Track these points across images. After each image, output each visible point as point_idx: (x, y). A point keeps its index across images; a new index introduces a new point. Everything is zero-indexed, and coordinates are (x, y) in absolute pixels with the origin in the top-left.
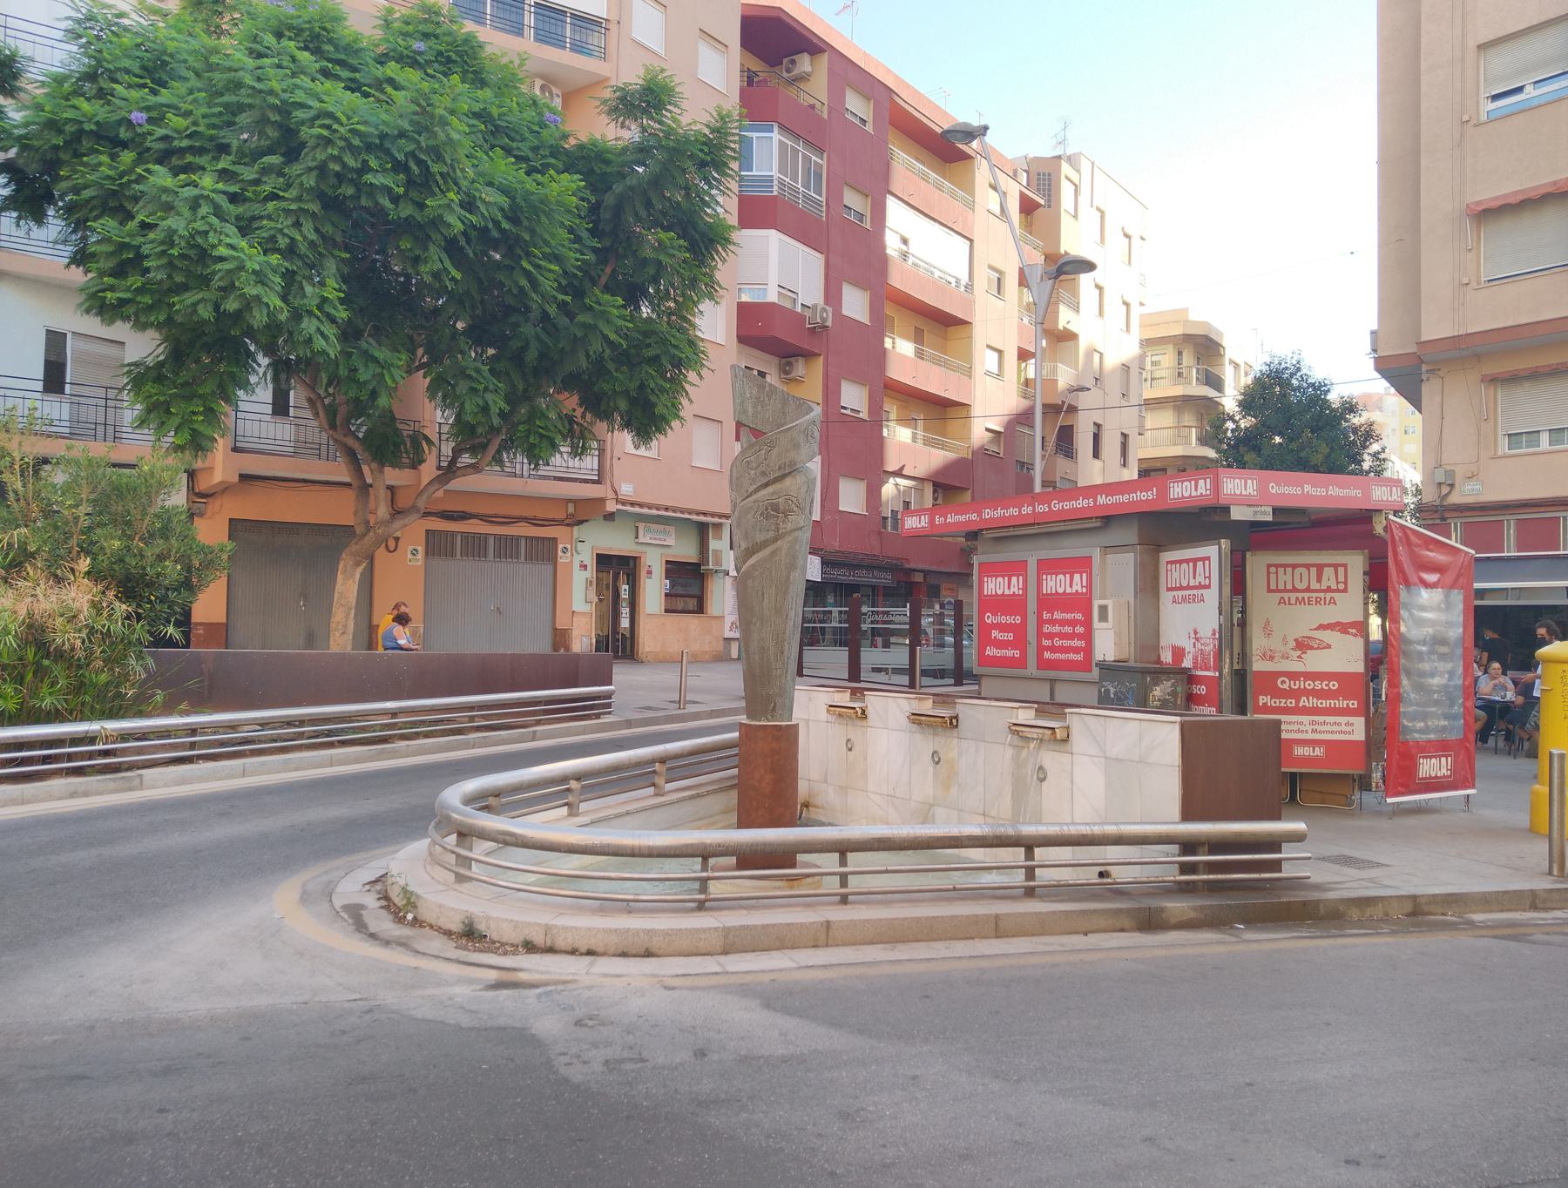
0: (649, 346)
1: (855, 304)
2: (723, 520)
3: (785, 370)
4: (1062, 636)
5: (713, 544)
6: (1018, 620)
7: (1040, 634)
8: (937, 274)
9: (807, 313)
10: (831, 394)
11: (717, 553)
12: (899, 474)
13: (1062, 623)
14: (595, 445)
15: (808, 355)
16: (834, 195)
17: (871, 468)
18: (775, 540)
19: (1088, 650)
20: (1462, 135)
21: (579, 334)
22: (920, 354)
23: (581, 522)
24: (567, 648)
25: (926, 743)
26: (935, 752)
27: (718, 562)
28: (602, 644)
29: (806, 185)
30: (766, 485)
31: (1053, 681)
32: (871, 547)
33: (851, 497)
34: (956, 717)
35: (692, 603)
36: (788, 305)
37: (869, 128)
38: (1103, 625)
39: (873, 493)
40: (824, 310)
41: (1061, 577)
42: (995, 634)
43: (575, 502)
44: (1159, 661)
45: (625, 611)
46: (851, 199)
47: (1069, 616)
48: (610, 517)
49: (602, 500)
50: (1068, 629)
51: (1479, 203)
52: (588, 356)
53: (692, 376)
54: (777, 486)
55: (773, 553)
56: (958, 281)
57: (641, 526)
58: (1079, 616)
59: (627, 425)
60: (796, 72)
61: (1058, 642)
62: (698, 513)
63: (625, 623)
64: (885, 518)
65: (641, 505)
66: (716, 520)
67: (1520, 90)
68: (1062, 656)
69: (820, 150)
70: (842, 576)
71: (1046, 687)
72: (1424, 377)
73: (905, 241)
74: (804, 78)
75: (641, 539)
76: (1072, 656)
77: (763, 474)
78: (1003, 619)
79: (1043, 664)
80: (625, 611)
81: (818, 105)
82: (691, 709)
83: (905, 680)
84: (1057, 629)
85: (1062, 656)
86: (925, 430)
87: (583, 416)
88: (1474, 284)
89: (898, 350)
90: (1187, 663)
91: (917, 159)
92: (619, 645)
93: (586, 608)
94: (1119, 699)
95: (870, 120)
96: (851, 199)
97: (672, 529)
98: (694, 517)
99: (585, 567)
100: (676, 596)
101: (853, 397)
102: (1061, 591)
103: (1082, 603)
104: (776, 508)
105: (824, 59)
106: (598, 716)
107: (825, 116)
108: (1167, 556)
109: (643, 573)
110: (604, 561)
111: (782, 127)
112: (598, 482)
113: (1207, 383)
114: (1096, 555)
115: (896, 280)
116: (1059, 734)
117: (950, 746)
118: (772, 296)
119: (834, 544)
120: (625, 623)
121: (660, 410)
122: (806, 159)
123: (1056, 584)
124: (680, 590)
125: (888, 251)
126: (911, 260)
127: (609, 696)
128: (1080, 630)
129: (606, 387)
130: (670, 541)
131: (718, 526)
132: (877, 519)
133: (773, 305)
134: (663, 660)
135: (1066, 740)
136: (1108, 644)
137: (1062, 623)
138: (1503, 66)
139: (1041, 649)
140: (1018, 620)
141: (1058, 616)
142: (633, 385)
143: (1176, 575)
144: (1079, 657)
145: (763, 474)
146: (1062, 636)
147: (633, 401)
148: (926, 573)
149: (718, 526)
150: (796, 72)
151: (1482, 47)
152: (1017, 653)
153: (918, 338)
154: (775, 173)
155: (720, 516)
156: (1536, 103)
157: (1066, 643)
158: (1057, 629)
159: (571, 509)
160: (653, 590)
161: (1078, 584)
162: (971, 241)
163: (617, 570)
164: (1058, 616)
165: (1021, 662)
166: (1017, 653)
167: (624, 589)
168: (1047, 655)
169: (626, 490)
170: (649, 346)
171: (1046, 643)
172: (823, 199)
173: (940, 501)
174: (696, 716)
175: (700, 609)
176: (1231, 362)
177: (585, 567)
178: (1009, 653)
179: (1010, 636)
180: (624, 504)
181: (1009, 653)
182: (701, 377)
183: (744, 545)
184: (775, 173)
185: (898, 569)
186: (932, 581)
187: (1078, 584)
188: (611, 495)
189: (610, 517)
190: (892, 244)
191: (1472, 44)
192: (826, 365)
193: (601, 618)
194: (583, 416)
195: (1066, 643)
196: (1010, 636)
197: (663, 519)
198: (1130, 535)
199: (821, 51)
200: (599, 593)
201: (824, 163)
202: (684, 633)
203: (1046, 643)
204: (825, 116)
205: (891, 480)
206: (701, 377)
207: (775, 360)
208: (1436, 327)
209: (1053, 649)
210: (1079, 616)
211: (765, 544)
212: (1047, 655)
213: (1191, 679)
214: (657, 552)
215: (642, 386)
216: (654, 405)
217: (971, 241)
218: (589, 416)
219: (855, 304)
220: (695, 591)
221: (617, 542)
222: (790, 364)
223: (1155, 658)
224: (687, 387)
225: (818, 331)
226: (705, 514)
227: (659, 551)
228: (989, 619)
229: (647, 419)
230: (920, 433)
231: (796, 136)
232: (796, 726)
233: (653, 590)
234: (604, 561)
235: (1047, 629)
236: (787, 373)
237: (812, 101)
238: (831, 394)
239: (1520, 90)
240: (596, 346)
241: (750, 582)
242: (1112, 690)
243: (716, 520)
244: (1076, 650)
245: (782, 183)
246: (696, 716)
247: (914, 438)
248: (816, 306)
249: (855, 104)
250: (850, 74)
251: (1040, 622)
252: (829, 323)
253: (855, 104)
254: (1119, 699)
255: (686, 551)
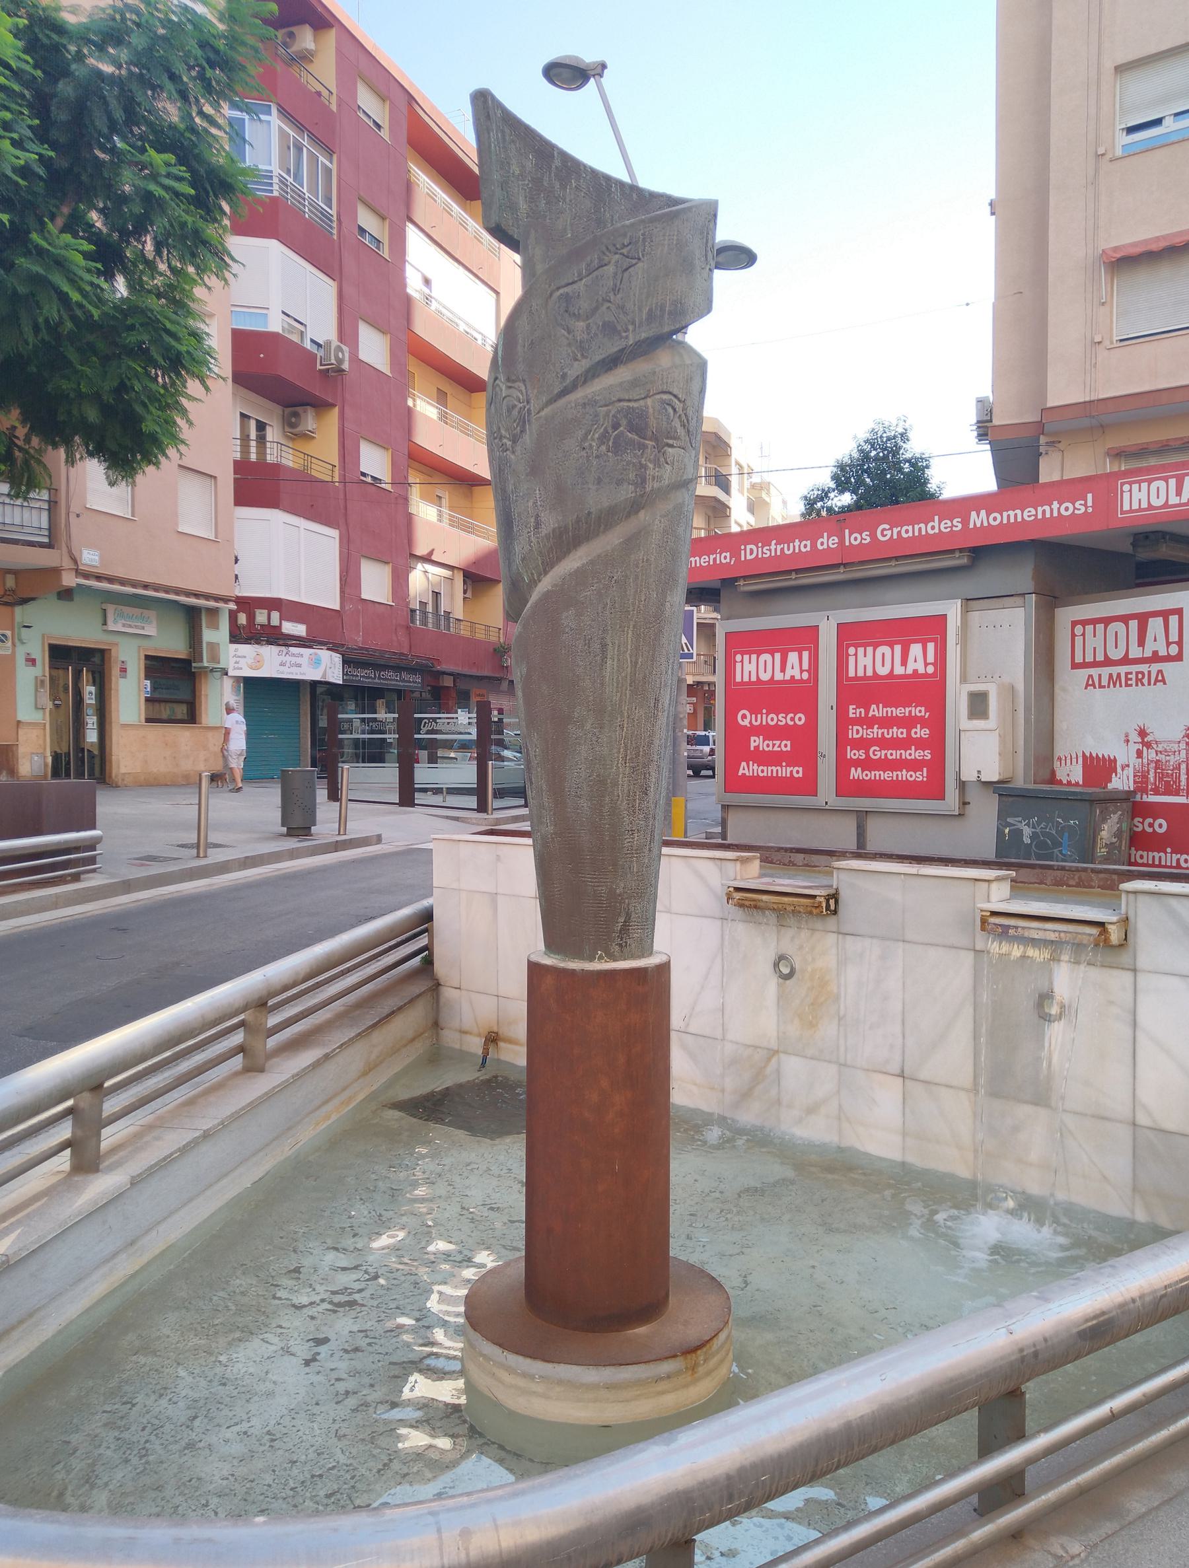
0: (132, 328)
1: (373, 349)
2: (220, 605)
3: (291, 423)
4: (884, 743)
5: (208, 635)
6: (801, 719)
7: (842, 741)
8: (462, 327)
9: (320, 353)
10: (348, 454)
11: (214, 647)
12: (427, 559)
13: (886, 722)
14: (45, 495)
15: (320, 406)
16: (346, 212)
17: (400, 551)
18: (635, 507)
19: (937, 766)
20: (1096, 171)
21: (22, 290)
22: (443, 417)
23: (24, 601)
24: (12, 772)
25: (760, 943)
26: (781, 958)
27: (215, 658)
28: (59, 766)
29: (313, 190)
30: (612, 363)
31: (862, 817)
32: (398, 644)
33: (375, 583)
34: (835, 896)
35: (181, 711)
36: (295, 338)
37: (385, 134)
38: (979, 723)
39: (400, 581)
40: (339, 349)
41: (766, 657)
42: (755, 742)
43: (16, 573)
44: (1052, 779)
45: (91, 721)
46: (366, 219)
47: (899, 712)
48: (66, 594)
49: (56, 572)
50: (897, 732)
51: (1115, 249)
52: (36, 329)
53: (193, 386)
54: (640, 367)
55: (631, 543)
56: (484, 338)
57: (111, 609)
58: (919, 711)
59: (99, 450)
60: (295, 48)
61: (876, 753)
62: (188, 593)
63: (92, 737)
64: (413, 611)
65: (111, 580)
66: (212, 604)
67: (1158, 122)
68: (886, 776)
69: (329, 151)
70: (364, 677)
71: (851, 825)
72: (1042, 449)
73: (427, 282)
74: (305, 57)
75: (111, 626)
76: (904, 775)
77: (610, 329)
78: (772, 719)
79: (845, 787)
80: (91, 721)
81: (325, 93)
82: (216, 856)
83: (472, 802)
84: (876, 732)
85: (886, 776)
86: (451, 508)
87: (28, 440)
88: (1107, 343)
89: (418, 408)
90: (1121, 782)
91: (442, 189)
92: (83, 765)
93: (37, 717)
94: (1041, 845)
95: (385, 122)
96: (366, 219)
97: (152, 614)
98: (182, 599)
99: (33, 662)
100: (159, 701)
101: (374, 462)
102: (765, 677)
103: (929, 691)
104: (638, 424)
105: (331, 36)
106: (76, 878)
107: (334, 107)
108: (1066, 615)
109: (115, 672)
110: (60, 654)
111: (284, 113)
112: (49, 546)
113: (718, 484)
114: (952, 610)
115: (421, 328)
116: (1115, 935)
117: (819, 948)
118: (275, 325)
119: (357, 639)
120: (92, 737)
121: (148, 426)
122: (313, 159)
123: (755, 668)
124: (164, 695)
125: (409, 291)
126: (434, 305)
127: (91, 845)
128: (920, 732)
129: (65, 385)
130: (151, 630)
131: (213, 612)
132: (401, 612)
133: (275, 336)
134: (152, 784)
135: (1124, 944)
136: (981, 751)
137: (886, 722)
138: (1145, 95)
139: (843, 765)
140: (801, 719)
141: (875, 711)
142: (109, 385)
143: (1091, 642)
144: (920, 776)
145: (610, 329)
146: (884, 743)
147: (107, 411)
148: (456, 676)
149: (213, 612)
150: (295, 48)
151: (1120, 69)
152: (798, 772)
153: (441, 398)
154: (276, 170)
155: (217, 599)
156: (1174, 138)
157: (893, 754)
158: (876, 732)
159: (10, 582)
160: (130, 694)
161: (919, 659)
162: (497, 293)
163: (80, 665)
164: (875, 711)
165: (809, 785)
166: (798, 772)
167: (89, 692)
168: (856, 773)
169: (90, 558)
170: (132, 328)
171: (852, 754)
172: (334, 212)
173: (469, 595)
174: (224, 868)
175: (192, 718)
176: (737, 463)
177: (33, 662)
178: (784, 771)
179: (786, 746)
180: (86, 576)
181: (784, 771)
182: (207, 389)
183: (550, 522)
184: (276, 170)
185: (429, 672)
186: (462, 686)
187: (919, 659)
188: (67, 563)
189: (66, 594)
190: (414, 284)
191: (1108, 65)
192: (342, 417)
193: (57, 731)
194: (28, 440)
195: (893, 754)
196: (786, 746)
197: (142, 600)
198: (1022, 576)
199: (330, 26)
200: (54, 697)
201: (334, 167)
202: (181, 748)
203: (852, 754)
204: (334, 107)
205: (420, 566)
206: (207, 389)
207: (278, 409)
208: (1064, 390)
209: (867, 764)
210: (919, 711)
211: (605, 521)
212: (856, 773)
213: (1142, 811)
214: (133, 642)
215: (122, 387)
216: (140, 420)
217: (497, 293)
218: (35, 441)
219: (373, 349)
220: (184, 695)
221: (78, 629)
222: (296, 415)
223: (1047, 776)
224: (184, 401)
225: (333, 375)
226: (197, 595)
227: (136, 642)
228: (745, 719)
229: (130, 442)
230: (445, 510)
231: (300, 127)
232: (663, 970)
233: (130, 694)
234: (60, 654)
235: (855, 732)
236: (292, 426)
237: (320, 88)
238: (348, 454)
239: (1158, 122)
240: (51, 311)
241: (568, 618)
242: (1027, 831)
243: (212, 604)
244: (914, 765)
245: (283, 181)
246: (224, 868)
247: (440, 515)
248: (329, 343)
249: (366, 100)
250: (361, 63)
251: (843, 722)
252: (346, 366)
253: (366, 100)
254: (1041, 845)
255: (173, 645)
